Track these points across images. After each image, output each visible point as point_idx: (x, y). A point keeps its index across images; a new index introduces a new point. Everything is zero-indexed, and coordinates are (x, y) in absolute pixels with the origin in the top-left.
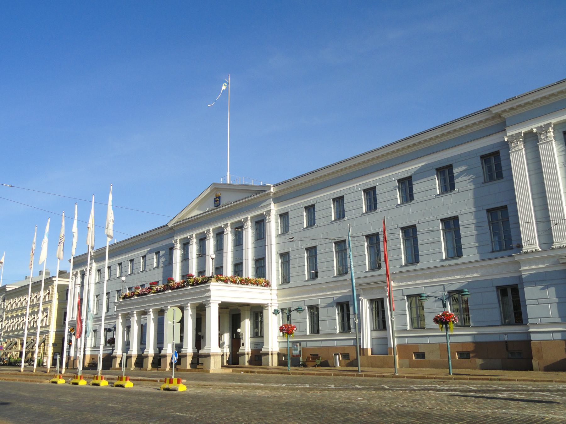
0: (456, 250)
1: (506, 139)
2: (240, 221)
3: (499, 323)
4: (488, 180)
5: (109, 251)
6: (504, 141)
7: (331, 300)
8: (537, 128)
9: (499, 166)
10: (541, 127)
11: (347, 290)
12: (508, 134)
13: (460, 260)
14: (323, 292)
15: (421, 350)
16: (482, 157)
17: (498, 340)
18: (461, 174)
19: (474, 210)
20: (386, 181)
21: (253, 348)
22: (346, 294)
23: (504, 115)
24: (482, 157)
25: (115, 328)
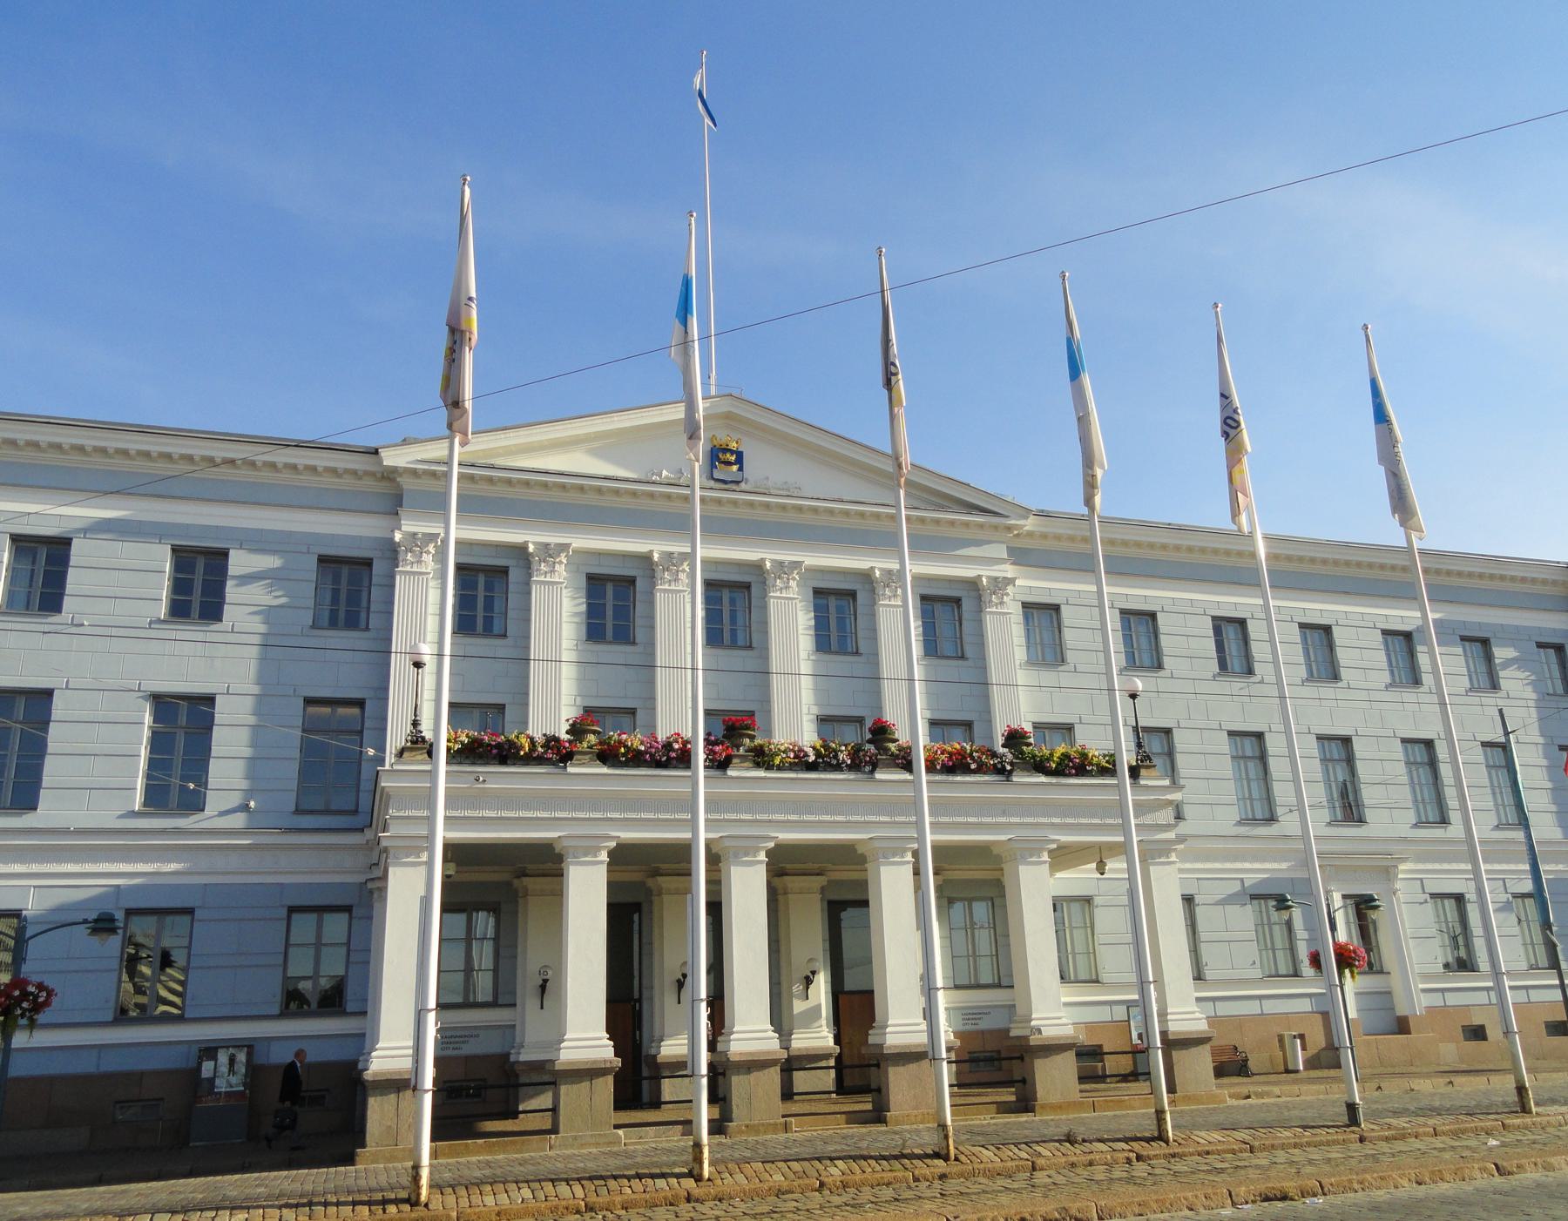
0: (1263, 811)
1: (398, 537)
2: (646, 558)
3: (276, 1011)
4: (326, 623)
5: (459, 495)
6: (392, 539)
7: (1237, 887)
8: (772, 561)
9: (354, 599)
10: (781, 563)
11: (1284, 866)
12: (404, 528)
13: (1273, 830)
14: (1264, 861)
15: (1477, 1021)
16: (323, 560)
17: (91, 1069)
18: (1508, 663)
19: (256, 689)
20: (1359, 623)
21: (961, 1028)
22: (1560, 876)
23: (406, 483)
24: (323, 560)
25: (103, 925)
